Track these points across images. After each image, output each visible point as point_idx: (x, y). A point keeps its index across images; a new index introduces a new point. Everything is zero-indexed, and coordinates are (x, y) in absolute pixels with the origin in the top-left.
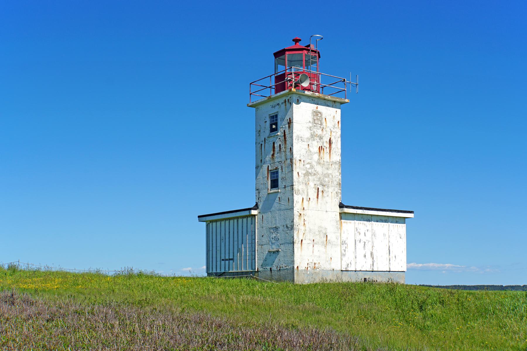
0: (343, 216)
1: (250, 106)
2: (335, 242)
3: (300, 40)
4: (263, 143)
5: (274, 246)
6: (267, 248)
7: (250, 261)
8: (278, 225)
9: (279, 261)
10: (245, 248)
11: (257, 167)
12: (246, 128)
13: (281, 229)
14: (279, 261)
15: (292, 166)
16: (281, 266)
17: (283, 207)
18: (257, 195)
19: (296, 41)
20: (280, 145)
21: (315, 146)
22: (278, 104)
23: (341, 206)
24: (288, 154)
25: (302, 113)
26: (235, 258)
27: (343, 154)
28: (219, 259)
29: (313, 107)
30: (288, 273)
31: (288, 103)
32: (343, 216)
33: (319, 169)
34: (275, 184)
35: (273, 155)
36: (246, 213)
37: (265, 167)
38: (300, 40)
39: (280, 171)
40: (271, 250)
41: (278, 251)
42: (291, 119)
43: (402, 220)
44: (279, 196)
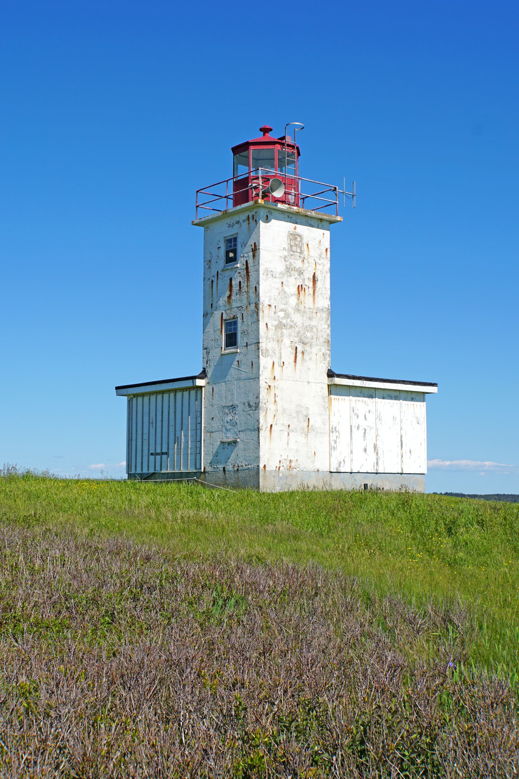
0: (333, 389)
1: (196, 225)
3: (271, 130)
4: (215, 279)
5: (229, 434)
6: (219, 437)
7: (193, 457)
8: (236, 402)
9: (237, 458)
10: (186, 436)
11: (205, 315)
12: (191, 254)
13: (240, 409)
16: (240, 464)
17: (243, 376)
18: (205, 356)
19: (265, 130)
20: (240, 282)
22: (238, 222)
23: (331, 374)
24: (252, 295)
25: (273, 236)
27: (332, 298)
30: (249, 477)
31: (253, 221)
32: (333, 389)
33: (297, 318)
35: (229, 297)
36: (189, 383)
38: (271, 130)
39: (239, 321)
40: (225, 440)
41: (235, 442)
42: (257, 244)
43: (420, 397)
44: (238, 358)
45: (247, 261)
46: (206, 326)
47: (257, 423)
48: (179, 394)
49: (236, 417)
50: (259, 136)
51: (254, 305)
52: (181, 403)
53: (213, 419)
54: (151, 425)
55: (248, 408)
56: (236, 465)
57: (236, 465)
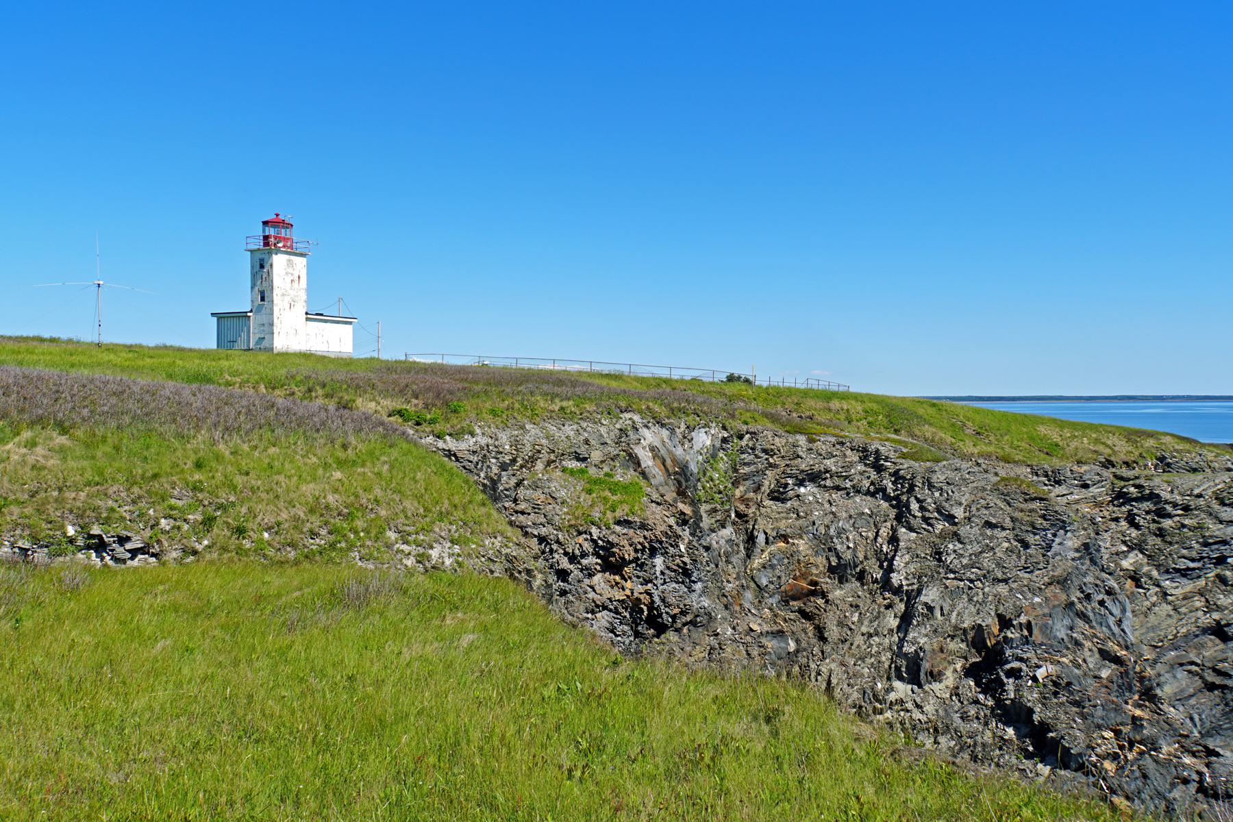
0: (307, 319)
2: (294, 332)
6: (258, 336)
9: (265, 344)
12: (245, 265)
14: (265, 344)
21: (289, 279)
25: (279, 261)
27: (308, 284)
29: (287, 257)
30: (270, 349)
31: (270, 253)
32: (307, 319)
33: (292, 293)
34: (262, 267)
43: (350, 323)
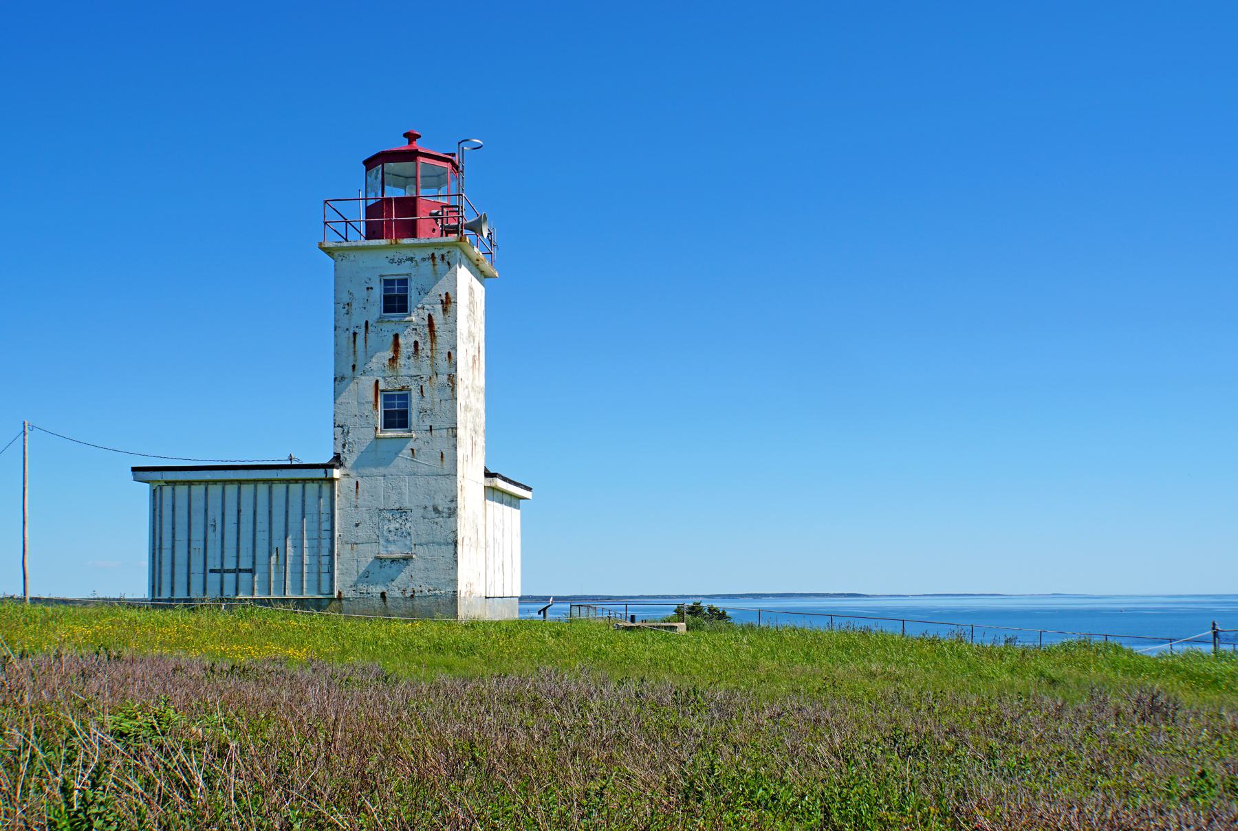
1: (324, 249)
3: (419, 136)
4: (361, 332)
5: (392, 548)
6: (368, 554)
7: (315, 577)
8: (407, 505)
9: (415, 579)
10: (299, 547)
11: (339, 379)
13: (418, 513)
15: (453, 389)
16: (417, 589)
17: (424, 469)
18: (340, 436)
19: (411, 137)
20: (416, 343)
22: (411, 259)
23: (488, 474)
24: (443, 364)
26: (258, 568)
28: (197, 567)
34: (397, 417)
35: (393, 360)
36: (320, 474)
37: (367, 383)
38: (419, 136)
39: (415, 395)
40: (384, 555)
41: (407, 559)
42: (451, 295)
44: (411, 444)
45: (430, 316)
46: (340, 394)
47: (451, 535)
48: (279, 489)
49: (408, 525)
50: (403, 145)
51: (446, 377)
52: (299, 500)
53: (357, 525)
54: (210, 530)
55: (433, 514)
56: (409, 590)
57: (409, 590)
